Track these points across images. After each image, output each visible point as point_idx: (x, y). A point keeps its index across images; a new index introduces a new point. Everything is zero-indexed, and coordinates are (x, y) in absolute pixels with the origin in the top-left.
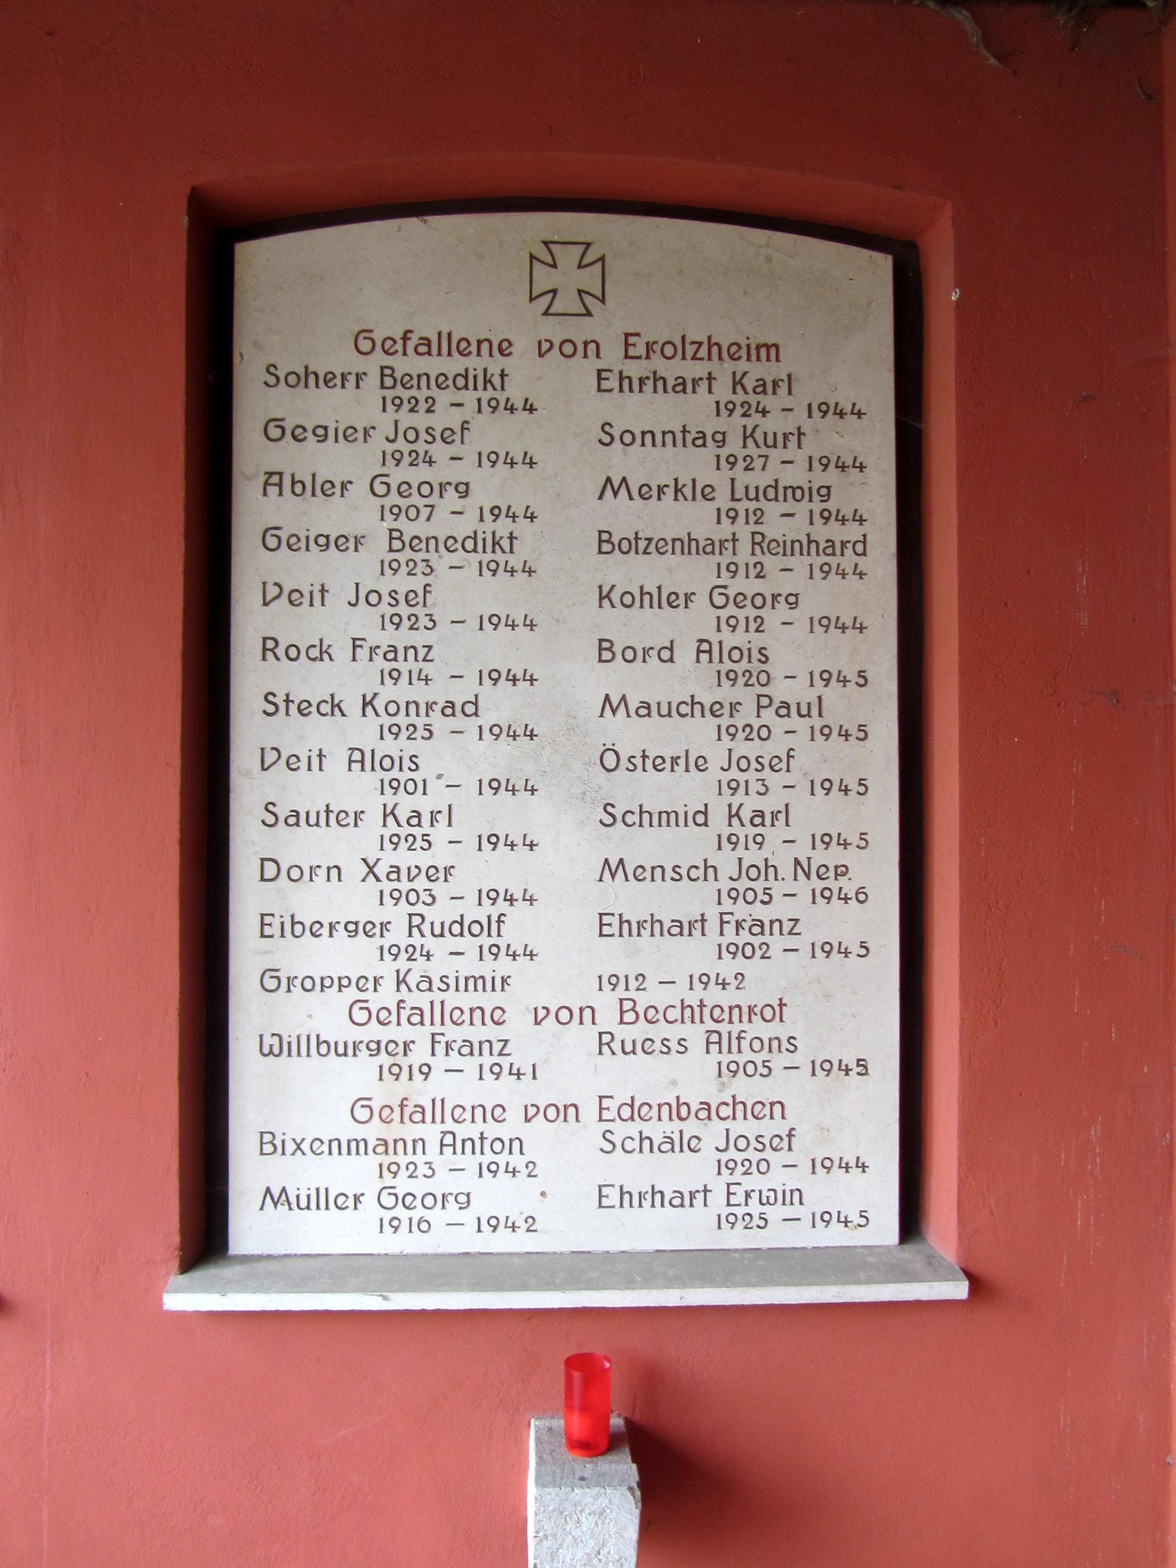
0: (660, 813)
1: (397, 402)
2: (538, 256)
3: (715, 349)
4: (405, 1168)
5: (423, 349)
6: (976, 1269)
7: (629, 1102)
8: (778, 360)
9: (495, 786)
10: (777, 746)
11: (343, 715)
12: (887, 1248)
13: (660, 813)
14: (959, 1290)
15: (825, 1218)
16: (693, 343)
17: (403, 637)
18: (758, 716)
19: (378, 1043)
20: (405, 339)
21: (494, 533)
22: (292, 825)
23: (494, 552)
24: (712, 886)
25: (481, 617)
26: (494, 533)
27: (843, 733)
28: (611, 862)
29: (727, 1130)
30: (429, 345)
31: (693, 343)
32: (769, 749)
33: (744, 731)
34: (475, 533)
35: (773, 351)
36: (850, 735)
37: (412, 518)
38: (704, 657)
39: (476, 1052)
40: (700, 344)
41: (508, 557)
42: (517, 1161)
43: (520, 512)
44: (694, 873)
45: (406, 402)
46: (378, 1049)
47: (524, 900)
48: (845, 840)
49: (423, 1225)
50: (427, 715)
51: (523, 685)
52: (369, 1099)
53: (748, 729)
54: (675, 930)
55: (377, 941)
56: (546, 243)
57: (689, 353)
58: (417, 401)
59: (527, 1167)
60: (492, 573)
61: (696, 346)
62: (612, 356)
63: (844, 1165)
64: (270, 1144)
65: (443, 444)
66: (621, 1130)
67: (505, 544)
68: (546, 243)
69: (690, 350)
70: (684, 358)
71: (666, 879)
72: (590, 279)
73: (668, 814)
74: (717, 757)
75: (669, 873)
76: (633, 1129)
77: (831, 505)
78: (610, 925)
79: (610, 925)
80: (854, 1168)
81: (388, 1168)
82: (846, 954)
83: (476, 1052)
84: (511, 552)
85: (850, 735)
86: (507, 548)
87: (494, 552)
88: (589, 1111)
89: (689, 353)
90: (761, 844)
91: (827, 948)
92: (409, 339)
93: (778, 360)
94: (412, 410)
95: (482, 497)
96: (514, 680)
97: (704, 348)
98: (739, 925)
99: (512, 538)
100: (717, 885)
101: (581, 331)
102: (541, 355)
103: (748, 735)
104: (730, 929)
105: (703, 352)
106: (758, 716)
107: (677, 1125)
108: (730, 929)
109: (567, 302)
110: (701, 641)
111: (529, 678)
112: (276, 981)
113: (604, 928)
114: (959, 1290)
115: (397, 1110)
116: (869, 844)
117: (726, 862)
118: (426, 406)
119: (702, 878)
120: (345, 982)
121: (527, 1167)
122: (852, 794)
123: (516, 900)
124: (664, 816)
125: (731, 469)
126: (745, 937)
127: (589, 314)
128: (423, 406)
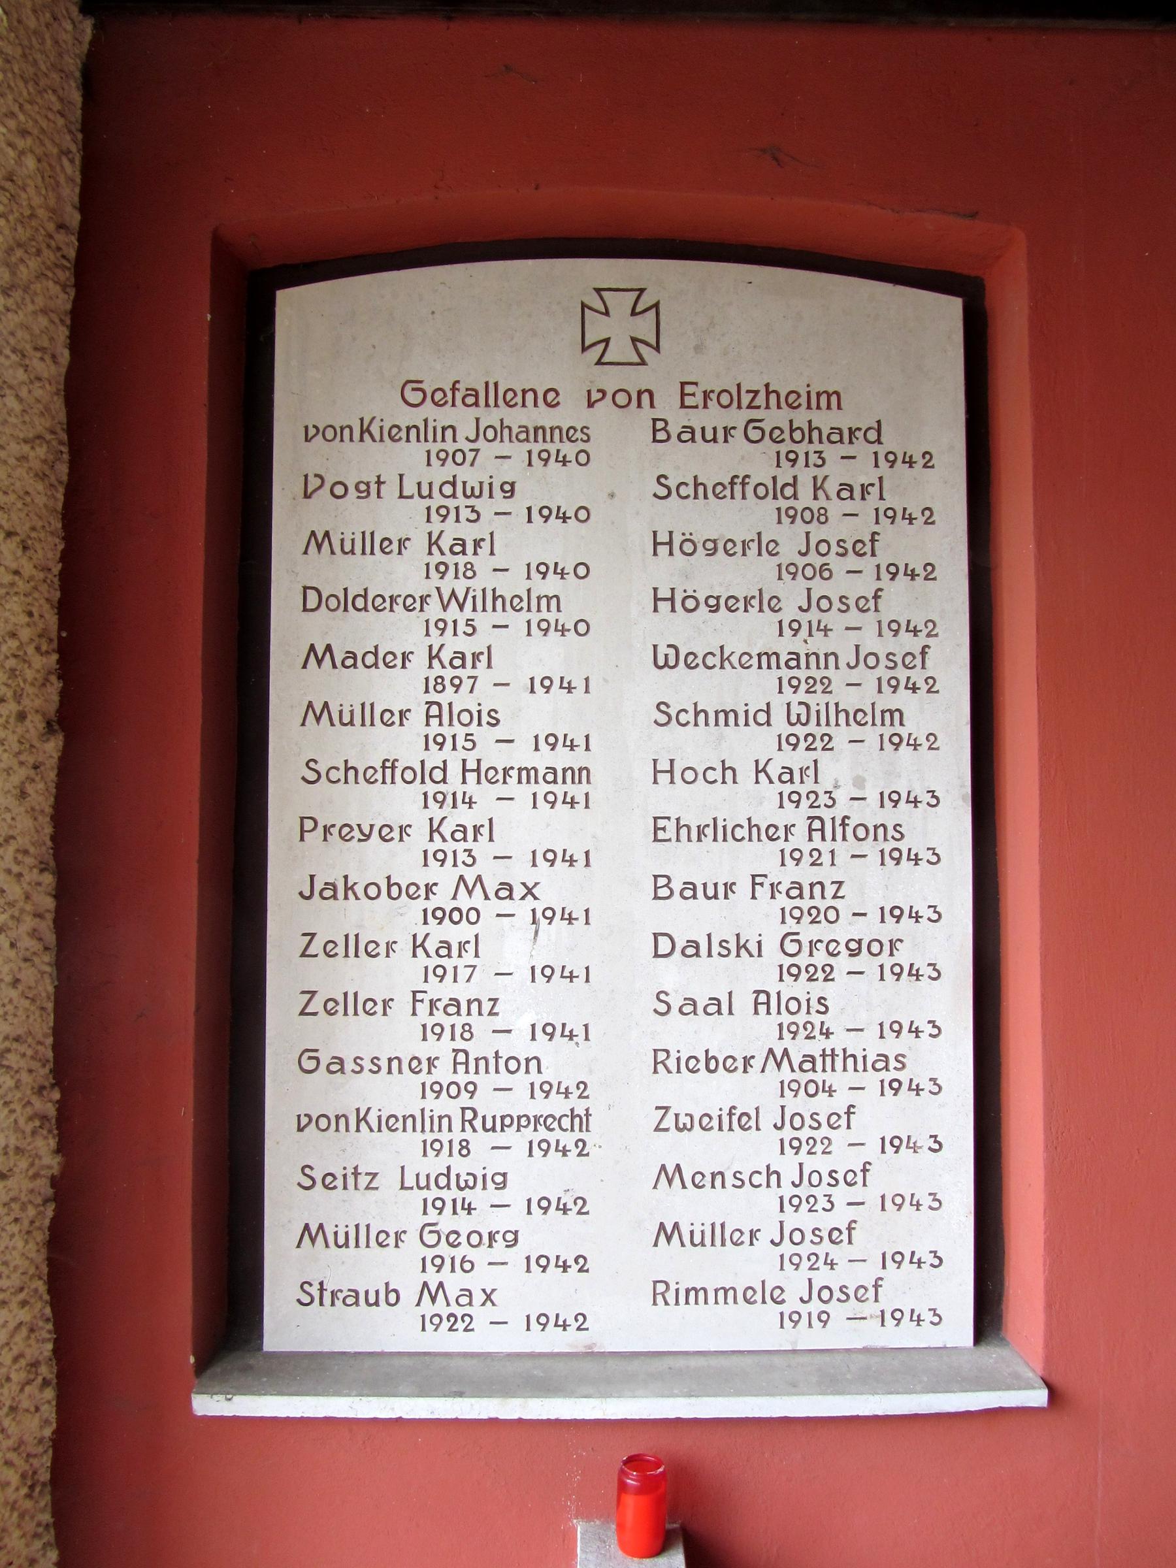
2: (590, 305)
3: (773, 397)
6: (1056, 1380)
8: (839, 407)
9: (548, 973)
12: (965, 1349)
14: (1038, 1397)
15: (897, 1316)
16: (748, 392)
24: (773, 1194)
25: (536, 737)
27: (914, 1087)
29: (801, 1165)
31: (748, 392)
33: (806, 740)
35: (834, 399)
36: (921, 917)
38: (762, 1009)
39: (560, 779)
40: (756, 392)
44: (757, 1179)
48: (910, 515)
53: (810, 739)
56: (598, 291)
57: (745, 401)
61: (752, 395)
62: (667, 406)
63: (913, 857)
65: (507, 408)
68: (598, 291)
69: (745, 400)
70: (739, 407)
71: (726, 1185)
72: (644, 327)
75: (730, 1180)
77: (899, 957)
78: (693, 395)
79: (693, 395)
82: (917, 918)
83: (560, 779)
85: (921, 917)
89: (745, 401)
90: (825, 1323)
91: (891, 457)
93: (839, 407)
97: (762, 394)
100: (780, 1019)
101: (634, 379)
103: (813, 803)
105: (761, 400)
109: (620, 350)
110: (758, 992)
113: (686, 398)
114: (1038, 1397)
116: (943, 1205)
119: (765, 1184)
122: (923, 863)
125: (793, 466)
127: (643, 363)
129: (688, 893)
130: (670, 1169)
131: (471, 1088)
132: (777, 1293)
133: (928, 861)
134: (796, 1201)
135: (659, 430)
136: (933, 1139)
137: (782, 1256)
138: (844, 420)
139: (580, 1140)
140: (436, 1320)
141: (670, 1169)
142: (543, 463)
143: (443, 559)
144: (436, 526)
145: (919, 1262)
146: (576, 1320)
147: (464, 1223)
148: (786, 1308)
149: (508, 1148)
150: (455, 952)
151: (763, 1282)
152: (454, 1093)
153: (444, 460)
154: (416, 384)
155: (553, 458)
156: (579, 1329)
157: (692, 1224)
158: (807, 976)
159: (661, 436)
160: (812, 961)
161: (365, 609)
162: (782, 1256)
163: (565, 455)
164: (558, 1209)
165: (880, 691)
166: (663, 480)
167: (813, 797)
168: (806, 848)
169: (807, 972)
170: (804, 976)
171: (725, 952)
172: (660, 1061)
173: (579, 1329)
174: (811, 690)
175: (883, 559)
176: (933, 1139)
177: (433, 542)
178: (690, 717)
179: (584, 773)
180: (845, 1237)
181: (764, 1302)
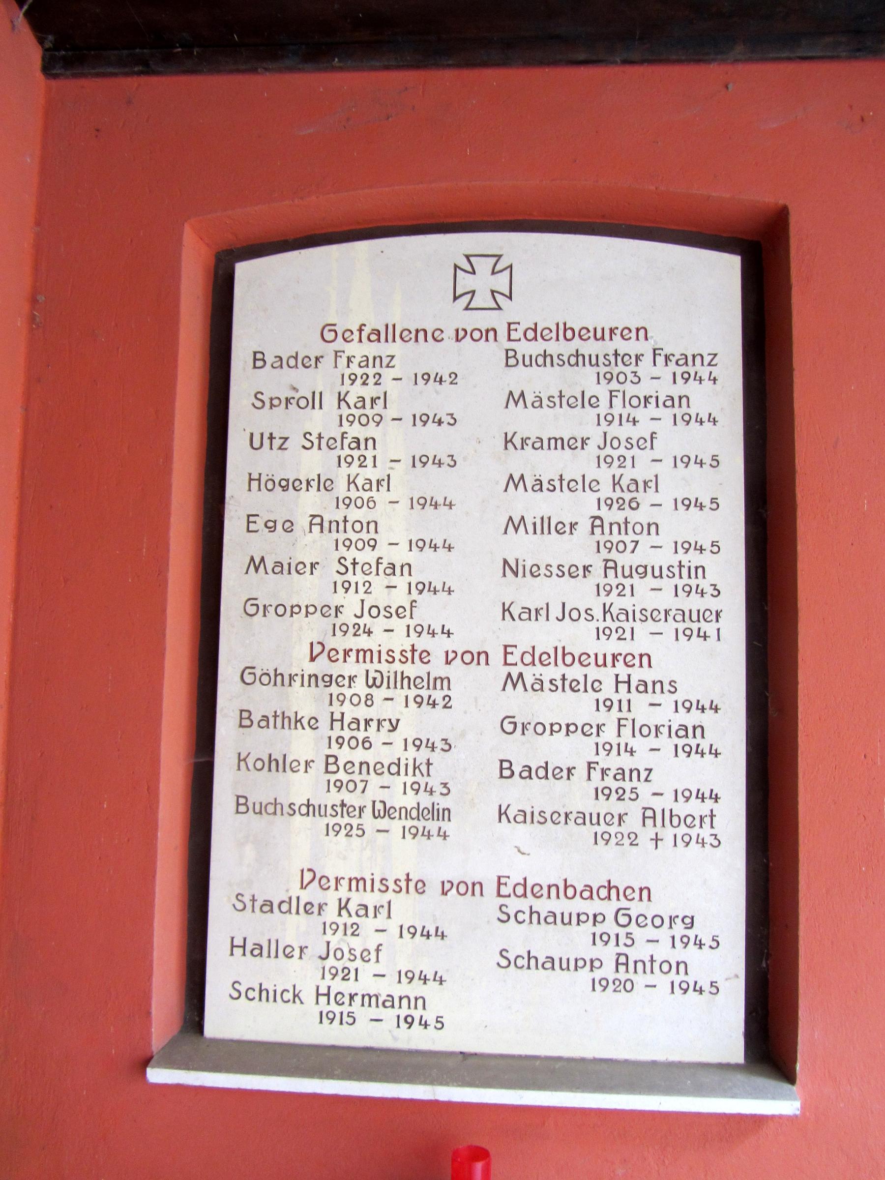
0: (549, 439)
1: (353, 377)
4: (352, 627)
5: (373, 337)
7: (533, 327)
10: (643, 430)
11: (302, 1003)
13: (549, 439)
17: (356, 430)
18: (617, 691)
19: (331, 676)
20: (360, 330)
21: (415, 760)
22: (270, 814)
23: (414, 775)
26: (415, 760)
28: (514, 405)
30: (379, 334)
32: (635, 432)
34: (399, 759)
37: (360, 499)
41: (426, 779)
42: (438, 695)
43: (440, 544)
45: (359, 377)
46: (331, 681)
47: (444, 547)
49: (367, 744)
50: (366, 730)
51: (443, 509)
52: (334, 325)
54: (548, 965)
55: (332, 620)
58: (368, 376)
59: (444, 699)
60: (422, 423)
64: (258, 360)
66: (514, 904)
67: (424, 768)
73: (556, 440)
74: (596, 439)
76: (523, 904)
80: (708, 709)
81: (345, 459)
84: (429, 775)
86: (425, 771)
87: (414, 775)
88: (490, 888)
92: (363, 330)
94: (364, 384)
95: (406, 731)
96: (436, 506)
98: (604, 772)
99: (429, 764)
102: (457, 340)
104: (596, 775)
106: (617, 691)
107: (562, 669)
108: (596, 775)
109: (482, 299)
111: (447, 590)
112: (333, 334)
115: (356, 334)
117: (605, 475)
118: (374, 381)
120: (311, 610)
121: (444, 699)
123: (439, 548)
124: (553, 442)
126: (609, 781)
128: (371, 381)
129: (525, 774)
130: (516, 478)
131: (372, 543)
132: (596, 684)
133: (711, 844)
134: (606, 836)
135: (510, 357)
136: (713, 587)
137: (599, 500)
138: (648, 675)
139: (447, 696)
140: (337, 828)
141: (516, 478)
142: (416, 748)
143: (350, 412)
144: (337, 709)
145: (701, 464)
146: (450, 377)
147: (359, 755)
148: (601, 696)
149: (397, 544)
150: (362, 446)
151: (584, 476)
152: (359, 505)
153: (340, 788)
154: (331, 326)
155: (431, 461)
156: (451, 383)
157: (535, 518)
158: (617, 796)
159: (512, 361)
160: (620, 829)
161: (296, 366)
162: (599, 500)
163: (441, 418)
164: (422, 935)
165: (676, 800)
166: (504, 953)
167: (621, 587)
168: (615, 698)
169: (618, 502)
170: (614, 796)
171: (554, 688)
172: (505, 769)
173: (451, 383)
174: (622, 465)
175: (680, 696)
176: (713, 587)
177: (341, 399)
178: (526, 917)
179: (446, 812)
180: (648, 444)
181: (586, 691)
